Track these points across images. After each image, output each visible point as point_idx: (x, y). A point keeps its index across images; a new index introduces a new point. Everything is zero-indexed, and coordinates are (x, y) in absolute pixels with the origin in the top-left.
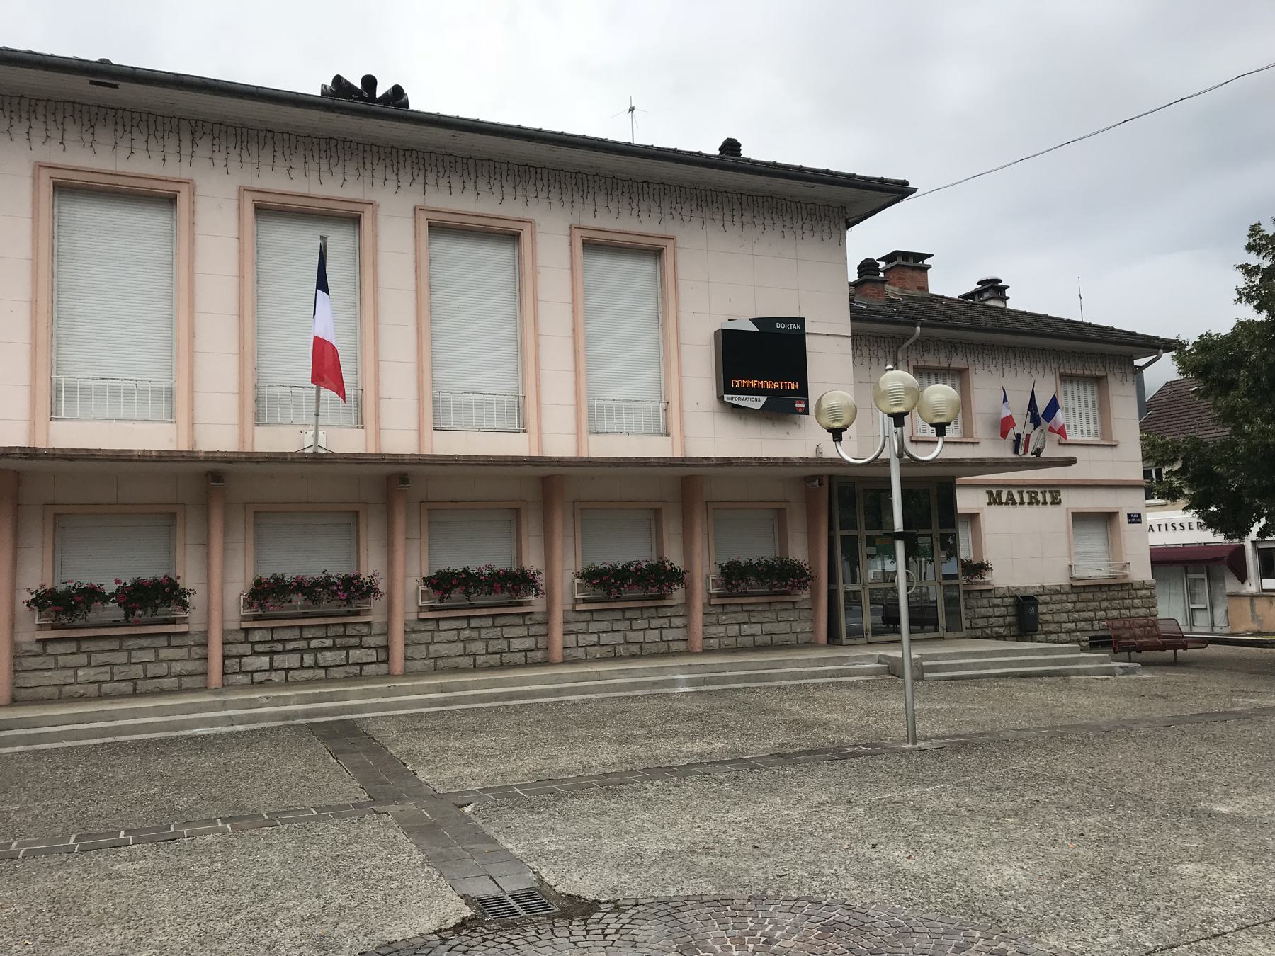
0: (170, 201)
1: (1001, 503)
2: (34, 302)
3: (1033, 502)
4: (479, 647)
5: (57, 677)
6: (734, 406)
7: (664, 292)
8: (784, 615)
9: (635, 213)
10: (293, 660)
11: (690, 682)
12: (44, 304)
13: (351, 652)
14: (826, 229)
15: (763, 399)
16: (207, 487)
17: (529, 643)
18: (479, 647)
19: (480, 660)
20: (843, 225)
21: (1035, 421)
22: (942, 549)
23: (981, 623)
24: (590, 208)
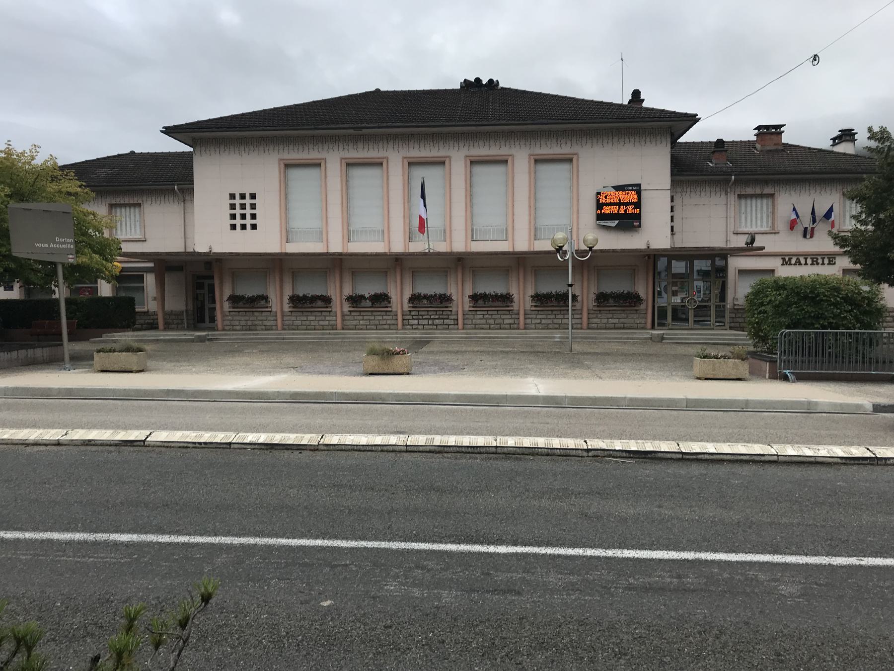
1: (790, 264)
2: (342, 203)
4: (492, 321)
5: (355, 322)
7: (575, 177)
8: (632, 316)
10: (426, 322)
11: (560, 338)
12: (345, 204)
15: (617, 222)
16: (396, 263)
17: (511, 321)
18: (492, 321)
19: (492, 326)
21: (814, 221)
24: (538, 145)
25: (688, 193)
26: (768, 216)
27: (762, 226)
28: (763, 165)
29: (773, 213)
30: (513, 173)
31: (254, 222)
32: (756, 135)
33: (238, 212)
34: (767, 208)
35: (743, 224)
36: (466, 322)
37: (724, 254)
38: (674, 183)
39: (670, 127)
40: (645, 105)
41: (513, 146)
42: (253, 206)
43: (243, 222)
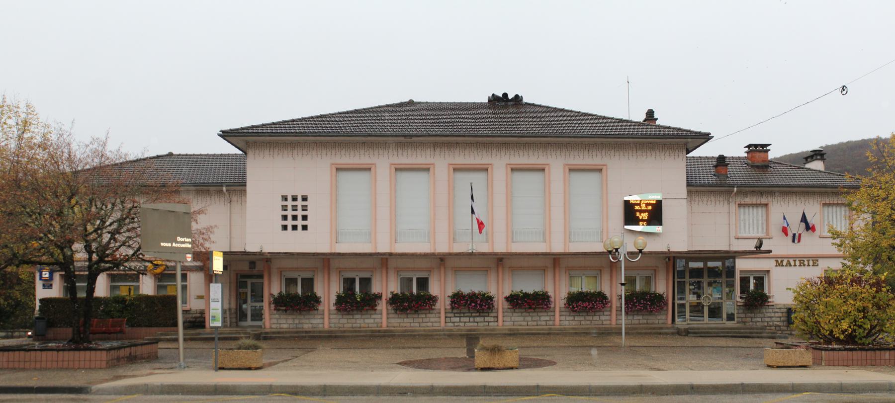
0: (428, 170)
3: (802, 264)
17: (548, 318)
23: (767, 320)
28: (754, 177)
31: (305, 223)
32: (747, 152)
33: (290, 213)
35: (742, 230)
36: (505, 319)
37: (730, 256)
38: (689, 192)
39: (686, 144)
40: (658, 123)
41: (549, 156)
42: (305, 208)
43: (295, 223)
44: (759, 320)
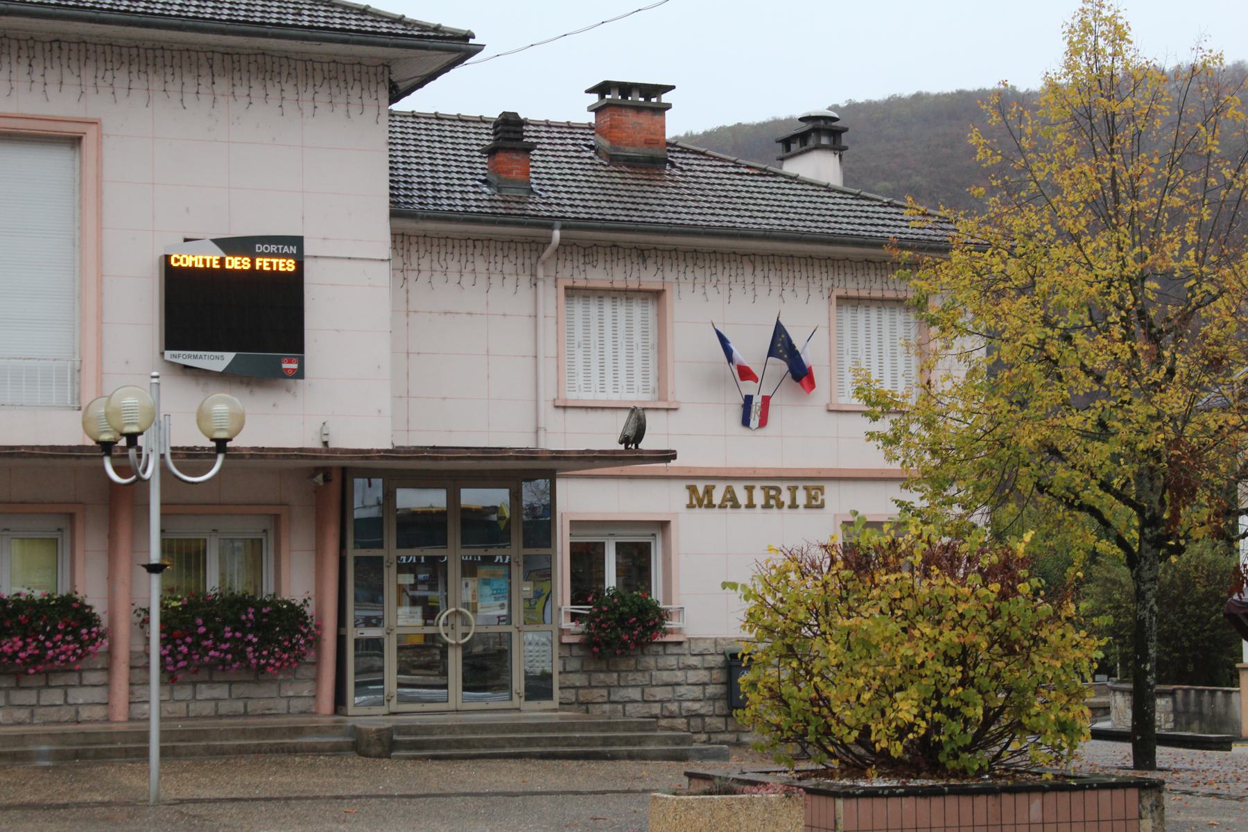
1: (710, 505)
6: (186, 367)
7: (88, 202)
9: (38, 87)
13: (220, 704)
14: (355, 99)
20: (384, 95)
22: (527, 579)
23: (660, 693)
25: (425, 276)
26: (645, 358)
27: (630, 388)
29: (661, 346)
30: (99, 178)
32: (597, 110)
34: (645, 333)
35: (580, 380)
44: (635, 694)
